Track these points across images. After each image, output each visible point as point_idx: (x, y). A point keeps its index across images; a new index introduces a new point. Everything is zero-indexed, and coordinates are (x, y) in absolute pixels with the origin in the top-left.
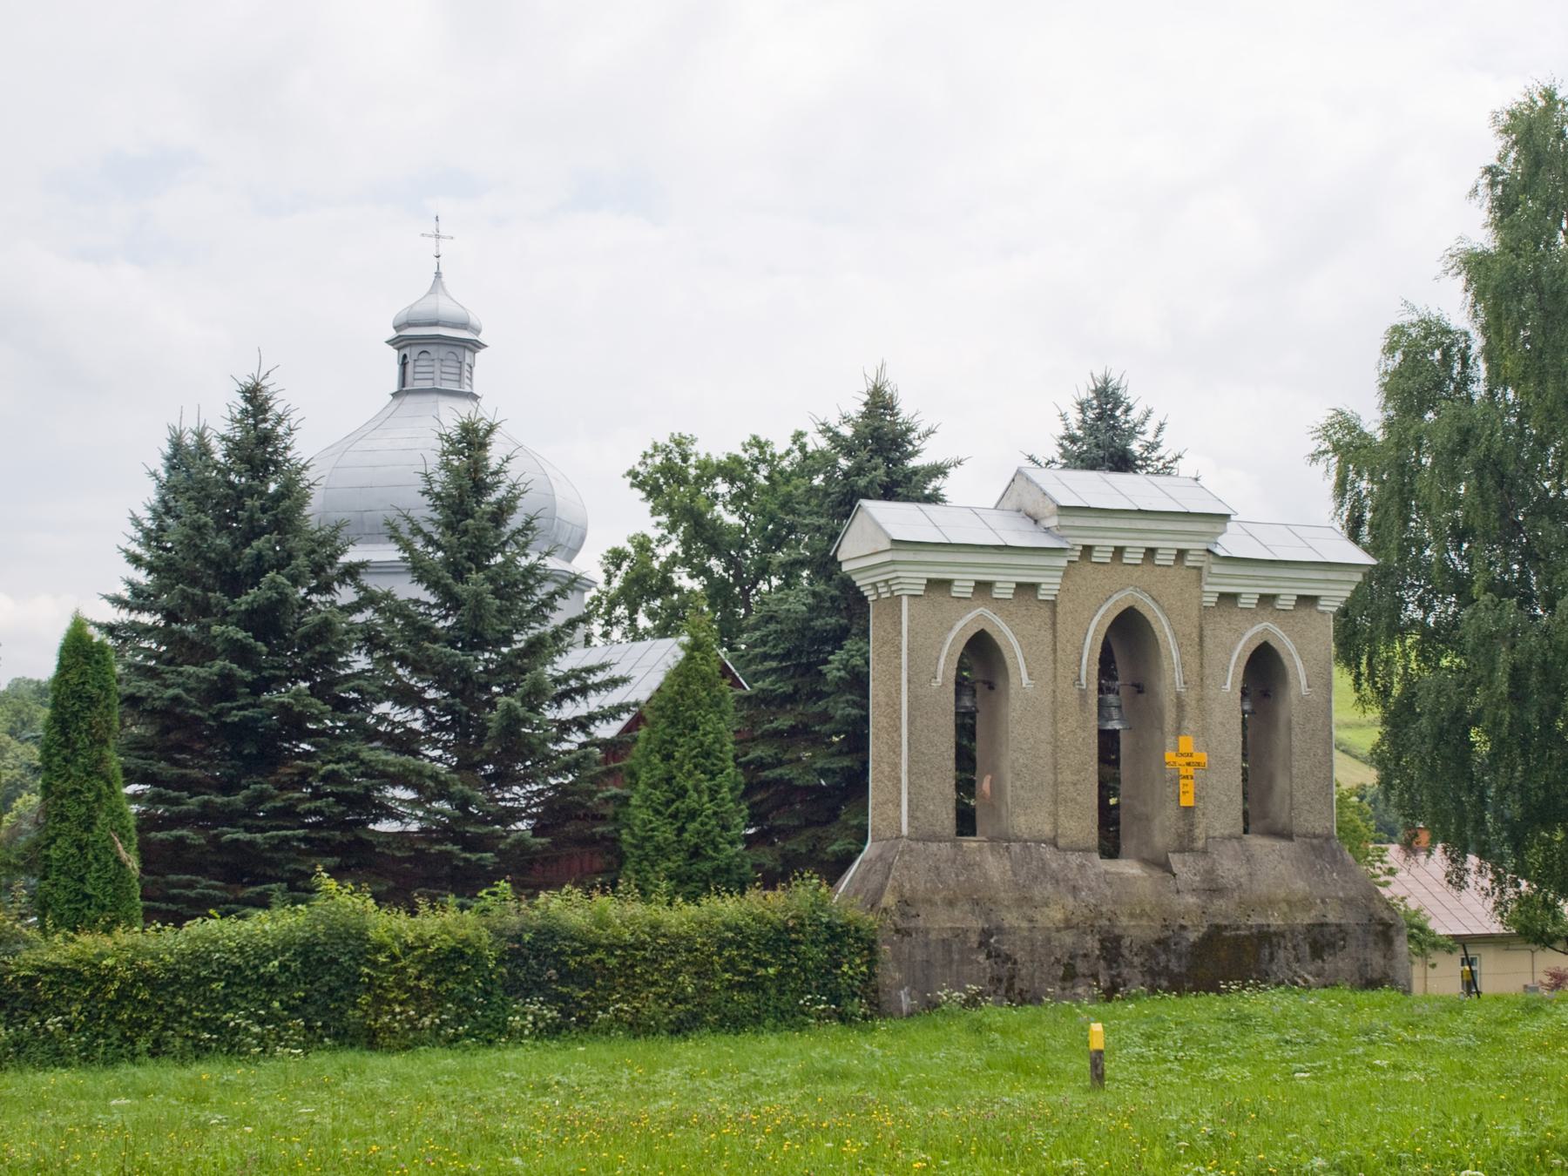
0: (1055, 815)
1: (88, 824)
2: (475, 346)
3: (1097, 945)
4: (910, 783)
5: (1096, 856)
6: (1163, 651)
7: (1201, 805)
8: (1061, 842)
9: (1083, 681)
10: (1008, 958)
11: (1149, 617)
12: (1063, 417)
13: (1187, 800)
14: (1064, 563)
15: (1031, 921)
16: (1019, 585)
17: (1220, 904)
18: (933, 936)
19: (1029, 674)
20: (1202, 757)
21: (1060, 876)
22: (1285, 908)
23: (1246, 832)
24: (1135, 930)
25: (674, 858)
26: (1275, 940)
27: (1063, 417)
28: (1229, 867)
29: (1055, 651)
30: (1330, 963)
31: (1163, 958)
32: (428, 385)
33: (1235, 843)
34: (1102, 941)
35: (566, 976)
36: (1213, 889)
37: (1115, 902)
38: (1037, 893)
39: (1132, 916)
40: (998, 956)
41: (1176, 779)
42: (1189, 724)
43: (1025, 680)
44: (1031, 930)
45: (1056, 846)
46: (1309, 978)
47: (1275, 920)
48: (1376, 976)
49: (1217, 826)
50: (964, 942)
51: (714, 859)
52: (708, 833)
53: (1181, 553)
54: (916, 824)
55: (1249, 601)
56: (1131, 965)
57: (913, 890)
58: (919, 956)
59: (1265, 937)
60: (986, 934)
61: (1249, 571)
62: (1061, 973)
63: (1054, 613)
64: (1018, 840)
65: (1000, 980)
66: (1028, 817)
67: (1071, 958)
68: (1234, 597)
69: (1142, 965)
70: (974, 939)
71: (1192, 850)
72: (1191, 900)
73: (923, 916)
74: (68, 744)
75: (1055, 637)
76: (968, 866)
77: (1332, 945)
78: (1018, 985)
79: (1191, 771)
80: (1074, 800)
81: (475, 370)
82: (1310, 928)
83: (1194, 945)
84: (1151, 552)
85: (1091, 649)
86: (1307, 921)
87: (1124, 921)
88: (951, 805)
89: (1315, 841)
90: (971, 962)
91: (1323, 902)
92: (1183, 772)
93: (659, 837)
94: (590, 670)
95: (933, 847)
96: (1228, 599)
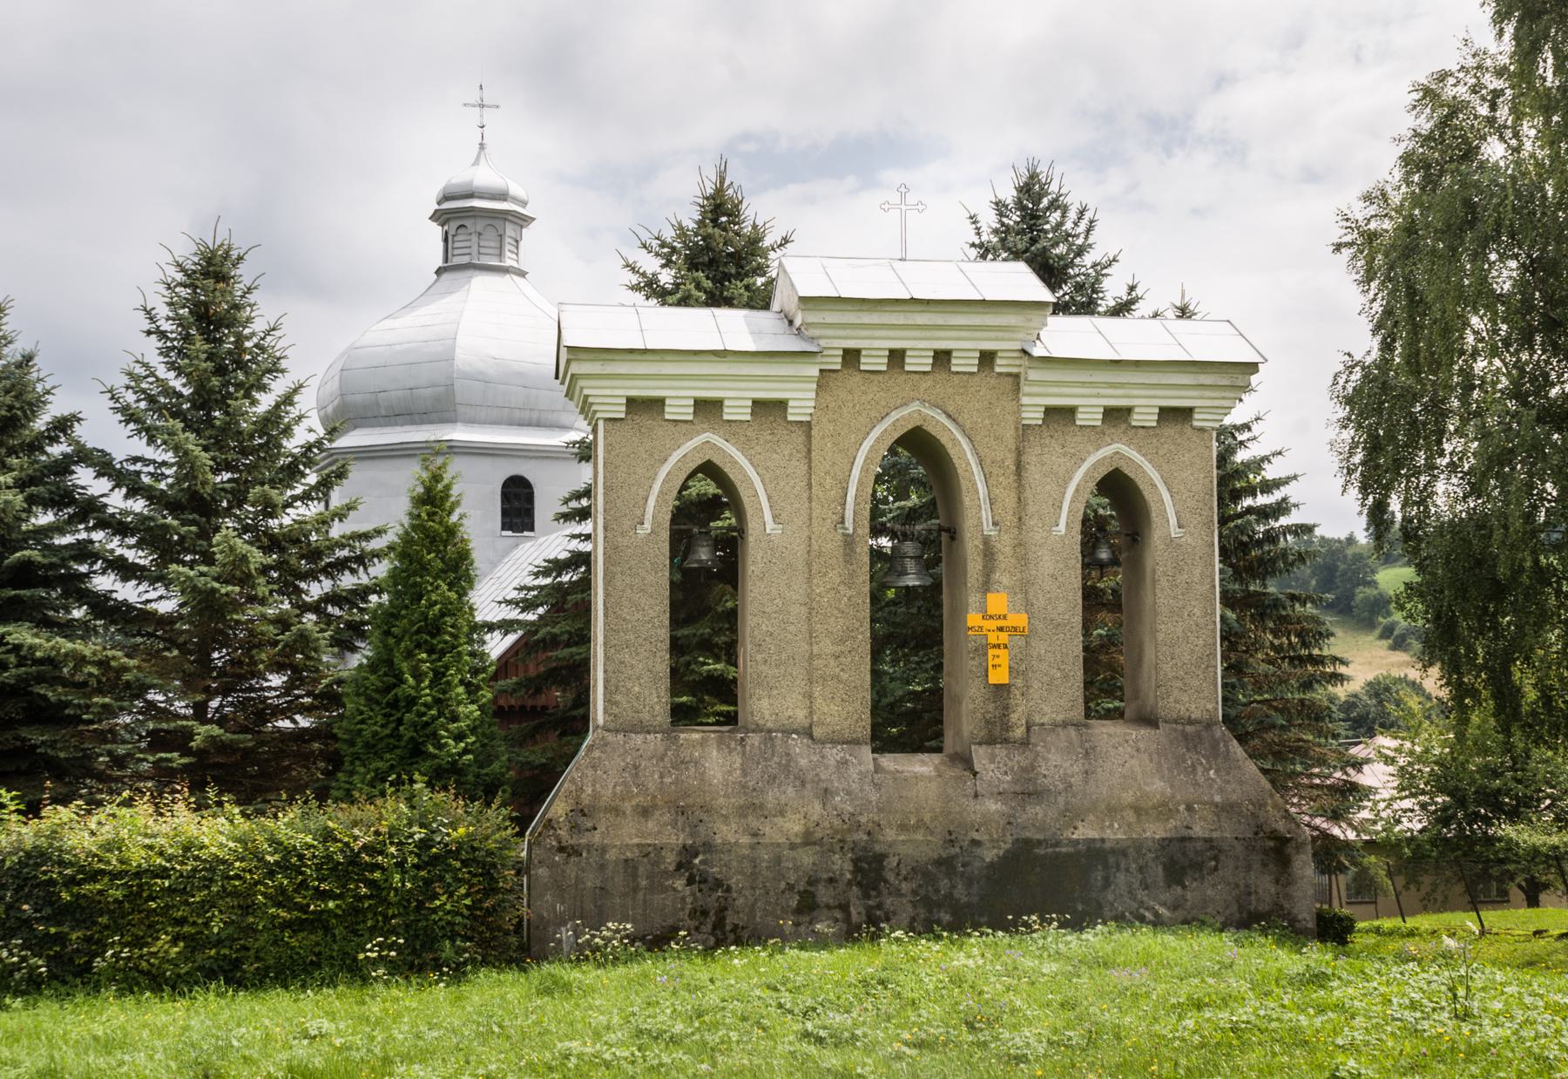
0: (809, 696)
2: (523, 221)
3: (848, 866)
4: (607, 658)
5: (866, 752)
6: (964, 484)
7: (1019, 682)
8: (818, 732)
9: (849, 524)
10: (718, 883)
11: (944, 440)
12: (974, 219)
13: (999, 676)
14: (814, 371)
15: (755, 835)
16: (757, 403)
17: (1036, 811)
18: (611, 855)
19: (775, 517)
20: (1020, 620)
21: (809, 777)
22: (1130, 816)
23: (1087, 716)
24: (905, 846)
25: (388, 756)
26: (1112, 860)
27: (974, 219)
28: (1056, 763)
29: (810, 485)
30: (1193, 891)
31: (944, 884)
32: (465, 260)
33: (1072, 731)
34: (855, 862)
35: (61, 913)
36: (1028, 791)
37: (880, 810)
38: (771, 798)
39: (903, 827)
40: (705, 881)
41: (982, 650)
42: (1002, 577)
43: (770, 525)
44: (752, 847)
45: (811, 737)
46: (1162, 910)
47: (1115, 833)
48: (1263, 908)
49: (1046, 709)
50: (656, 863)
51: (435, 757)
52: (427, 724)
53: (987, 358)
54: (615, 710)
55: (1089, 415)
56: (898, 893)
57: (596, 796)
58: (591, 881)
59: (1096, 855)
60: (688, 852)
61: (1083, 376)
62: (794, 903)
63: (809, 437)
64: (758, 729)
65: (705, 913)
67: (810, 883)
68: (1070, 412)
69: (915, 893)
70: (670, 860)
71: (1006, 741)
72: (993, 806)
73: (601, 828)
75: (810, 468)
76: (681, 764)
77: (1198, 866)
78: (731, 919)
79: (1004, 638)
80: (837, 678)
81: (522, 244)
82: (1165, 843)
83: (992, 864)
84: (897, 357)
85: (860, 483)
86: (1160, 834)
87: (890, 834)
89: (1189, 729)
90: (665, 889)
91: (1189, 808)
92: (992, 639)
94: (366, 536)
95: (638, 739)
96: (1060, 415)
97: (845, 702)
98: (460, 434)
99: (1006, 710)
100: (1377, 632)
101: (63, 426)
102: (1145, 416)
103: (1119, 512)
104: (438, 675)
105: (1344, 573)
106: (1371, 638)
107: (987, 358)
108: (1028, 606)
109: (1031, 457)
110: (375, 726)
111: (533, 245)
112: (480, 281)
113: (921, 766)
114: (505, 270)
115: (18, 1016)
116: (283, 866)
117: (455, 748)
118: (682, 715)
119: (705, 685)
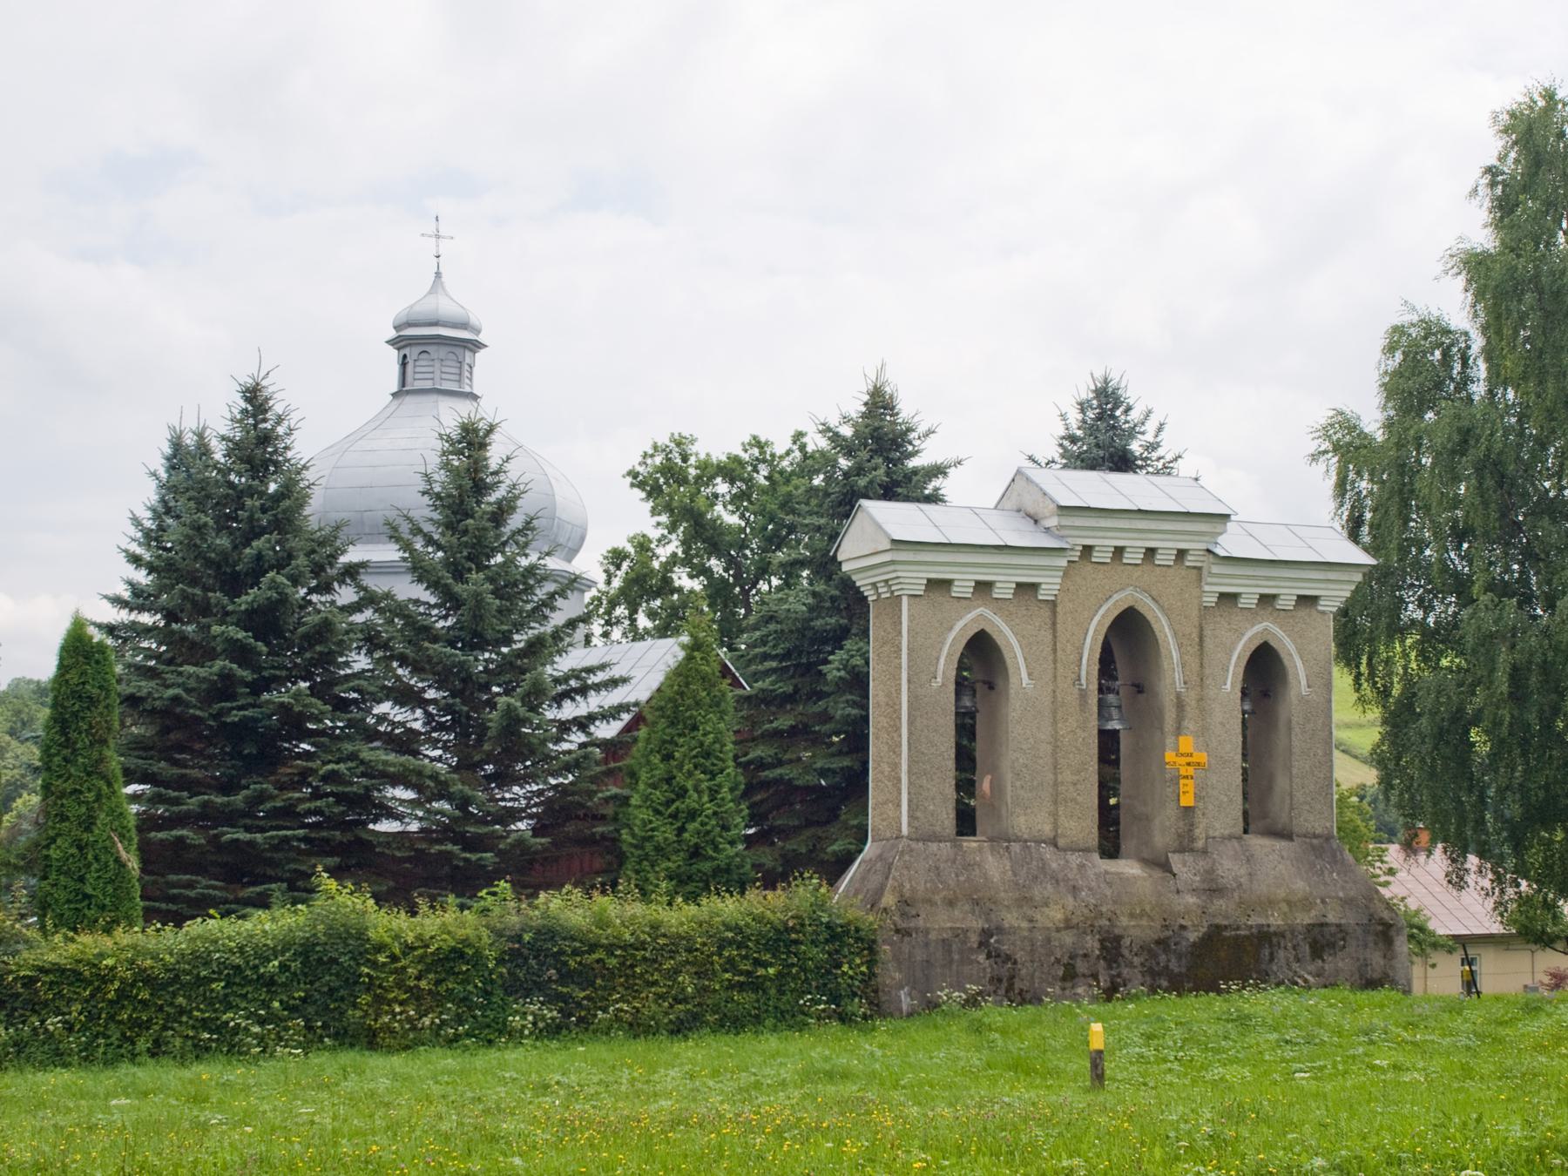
0: (1055, 815)
1: (88, 824)
2: (475, 346)
3: (1097, 945)
4: (910, 783)
5: (1096, 856)
6: (1163, 651)
7: (1201, 805)
8: (1061, 842)
9: (1083, 681)
10: (1008, 958)
11: (1149, 617)
12: (1063, 417)
13: (1187, 800)
14: (1064, 563)
15: (1031, 921)
16: (1019, 585)
17: (1220, 904)
18: (933, 936)
19: (1029, 674)
20: (1202, 757)
21: (1060, 876)
22: (1285, 908)
23: (1246, 832)
24: (1135, 930)
25: (674, 858)
26: (1275, 940)
27: (1063, 417)
28: (1229, 867)
29: (1055, 651)
30: (1330, 963)
31: (1163, 958)
32: (428, 385)
33: (1235, 843)
34: (1102, 941)
35: (566, 976)
36: (1213, 889)
37: (1115, 902)
38: (1037, 893)
39: (1132, 916)
40: (998, 956)
41: (1176, 779)
42: (1189, 724)
43: (1025, 680)
44: (1031, 930)
45: (1056, 846)
46: (1309, 978)
47: (1275, 920)
48: (1376, 976)
49: (1217, 826)
50: (964, 942)
51: (714, 859)
52: (708, 833)
53: (1181, 553)
54: (916, 824)
55: (1249, 601)
56: (1131, 965)
57: (913, 890)
58: (919, 956)
59: (1265, 937)
60: (986, 934)
61: (1249, 571)
62: (1061, 973)
63: (1054, 613)
64: (1018, 840)
65: (1000, 980)
66: (1028, 817)
67: (1071, 958)
68: (1234, 597)
69: (1142, 965)
70: (974, 939)
71: (1192, 850)
72: (1191, 900)
73: (923, 916)
74: (68, 744)
75: (1055, 637)
76: (968, 866)
77: (1332, 945)
78: (1018, 985)
79: (1191, 771)
80: (1074, 800)
81: (475, 370)
82: (1310, 928)
83: (1194, 945)
84: (1151, 552)
85: (1091, 649)
86: (1307, 921)
87: (1124, 921)
88: (951, 805)
89: (1315, 841)
90: (971, 962)
91: (1323, 902)
92: (1183, 772)
93: (659, 837)
94: (590, 670)
95: (933, 847)
96: (1228, 599)
115: (10, 1077)
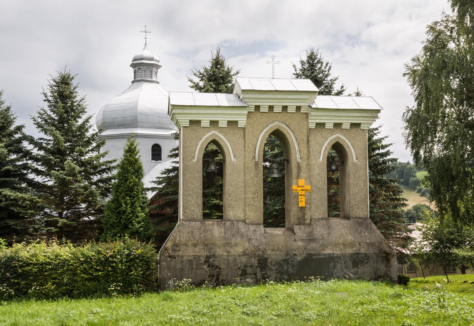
0: (245, 210)
2: (158, 67)
3: (256, 262)
4: (183, 199)
5: (262, 227)
6: (291, 146)
7: (308, 206)
8: (247, 221)
9: (257, 158)
10: (217, 267)
11: (285, 133)
12: (294, 66)
13: (302, 204)
14: (246, 112)
15: (228, 252)
16: (229, 122)
17: (313, 245)
18: (185, 258)
19: (234, 156)
20: (308, 187)
21: (245, 235)
22: (342, 247)
23: (329, 216)
24: (274, 256)
25: (117, 228)
26: (336, 260)
27: (294, 66)
28: (319, 231)
29: (245, 147)
30: (361, 269)
31: (285, 267)
32: (141, 78)
33: (324, 221)
34: (259, 260)
35: (18, 276)
36: (311, 239)
37: (266, 245)
38: (233, 241)
39: (273, 250)
40: (213, 266)
41: (297, 196)
42: (303, 174)
43: (233, 158)
44: (227, 256)
45: (245, 223)
46: (351, 275)
47: (337, 252)
48: (382, 274)
49: (316, 214)
50: (198, 261)
51: (132, 229)
52: (129, 219)
53: (298, 108)
54: (186, 215)
55: (329, 125)
56: (271, 270)
57: (180, 240)
58: (179, 266)
59: (331, 258)
60: (208, 257)
61: (327, 114)
62: (240, 273)
63: (245, 132)
64: (229, 220)
65: (213, 276)
67: (245, 267)
68: (323, 124)
69: (277, 270)
70: (203, 260)
71: (304, 224)
72: (300, 244)
73: (182, 250)
75: (245, 141)
76: (206, 231)
77: (362, 262)
78: (221, 278)
79: (303, 193)
80: (253, 205)
81: (158, 74)
82: (352, 255)
83: (300, 261)
84: (271, 108)
85: (260, 146)
86: (351, 252)
87: (269, 252)
89: (359, 220)
90: (201, 269)
91: (360, 244)
92: (300, 193)
94: (111, 162)
95: (193, 223)
96: (320, 125)
97: (255, 212)
98: (139, 131)
99: (304, 214)
100: (416, 191)
101: (19, 129)
102: (346, 126)
103: (338, 155)
104: (133, 204)
105: (406, 173)
106: (414, 193)
107: (298, 108)
108: (311, 183)
109: (312, 138)
110: (113, 219)
111: (161, 74)
112: (145, 85)
113: (278, 231)
114: (153, 82)
116: (85, 262)
117: (137, 226)
118: (206, 216)
119: (213, 207)
